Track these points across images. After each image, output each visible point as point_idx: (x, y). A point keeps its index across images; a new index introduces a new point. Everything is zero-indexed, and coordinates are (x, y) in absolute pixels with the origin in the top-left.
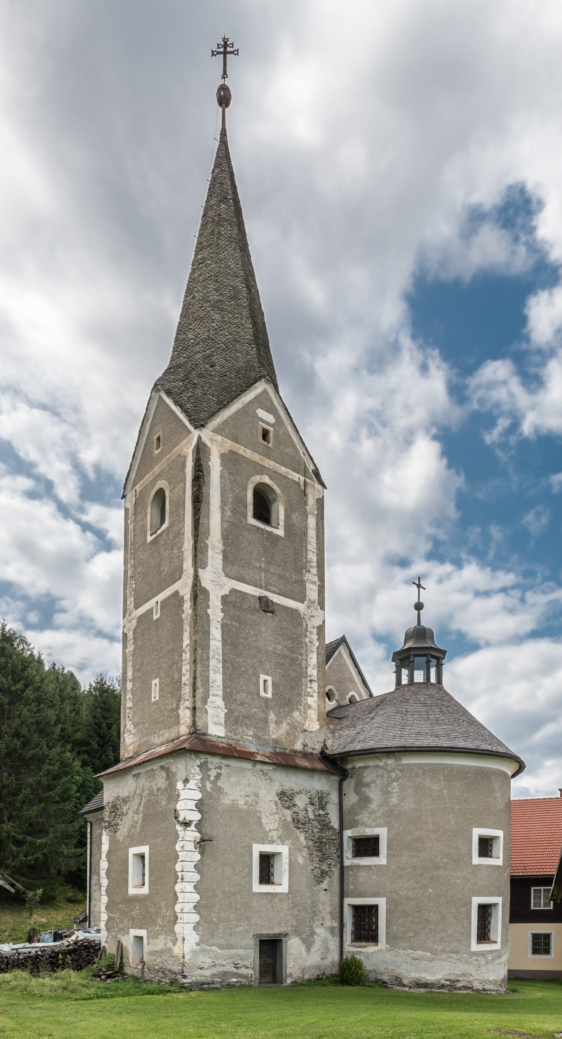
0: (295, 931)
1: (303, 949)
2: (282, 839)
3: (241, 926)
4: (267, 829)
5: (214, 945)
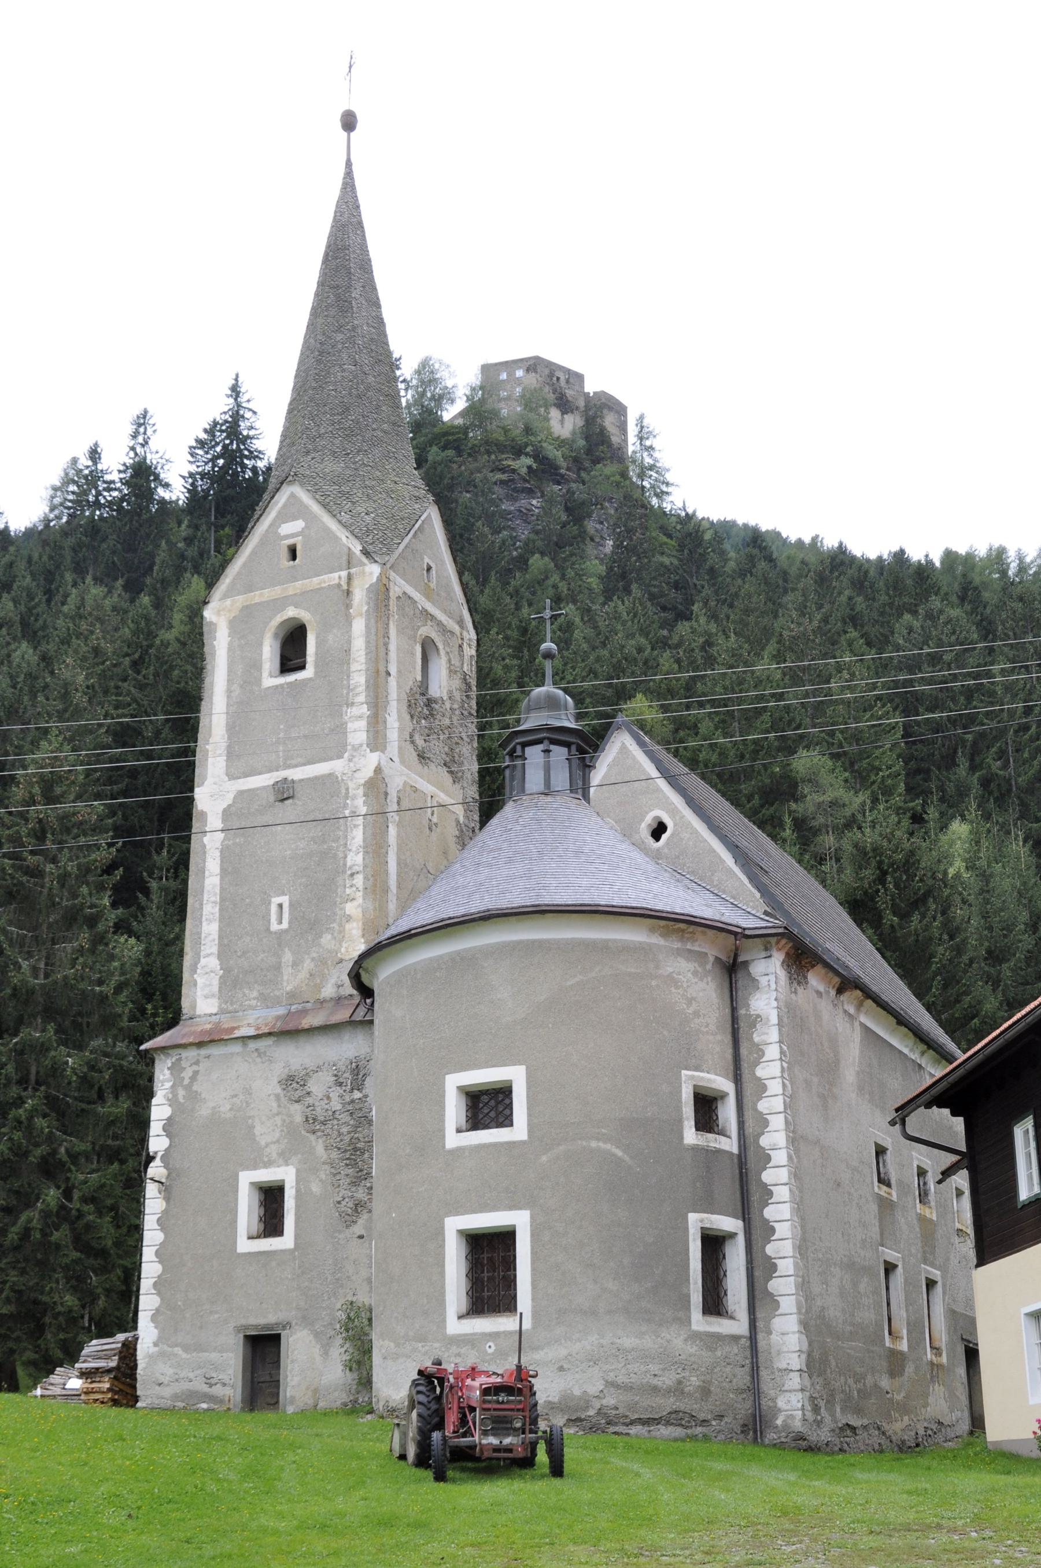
0: (304, 1317)
1: (316, 1351)
2: (285, 1158)
3: (216, 1312)
4: (263, 1143)
5: (177, 1346)
